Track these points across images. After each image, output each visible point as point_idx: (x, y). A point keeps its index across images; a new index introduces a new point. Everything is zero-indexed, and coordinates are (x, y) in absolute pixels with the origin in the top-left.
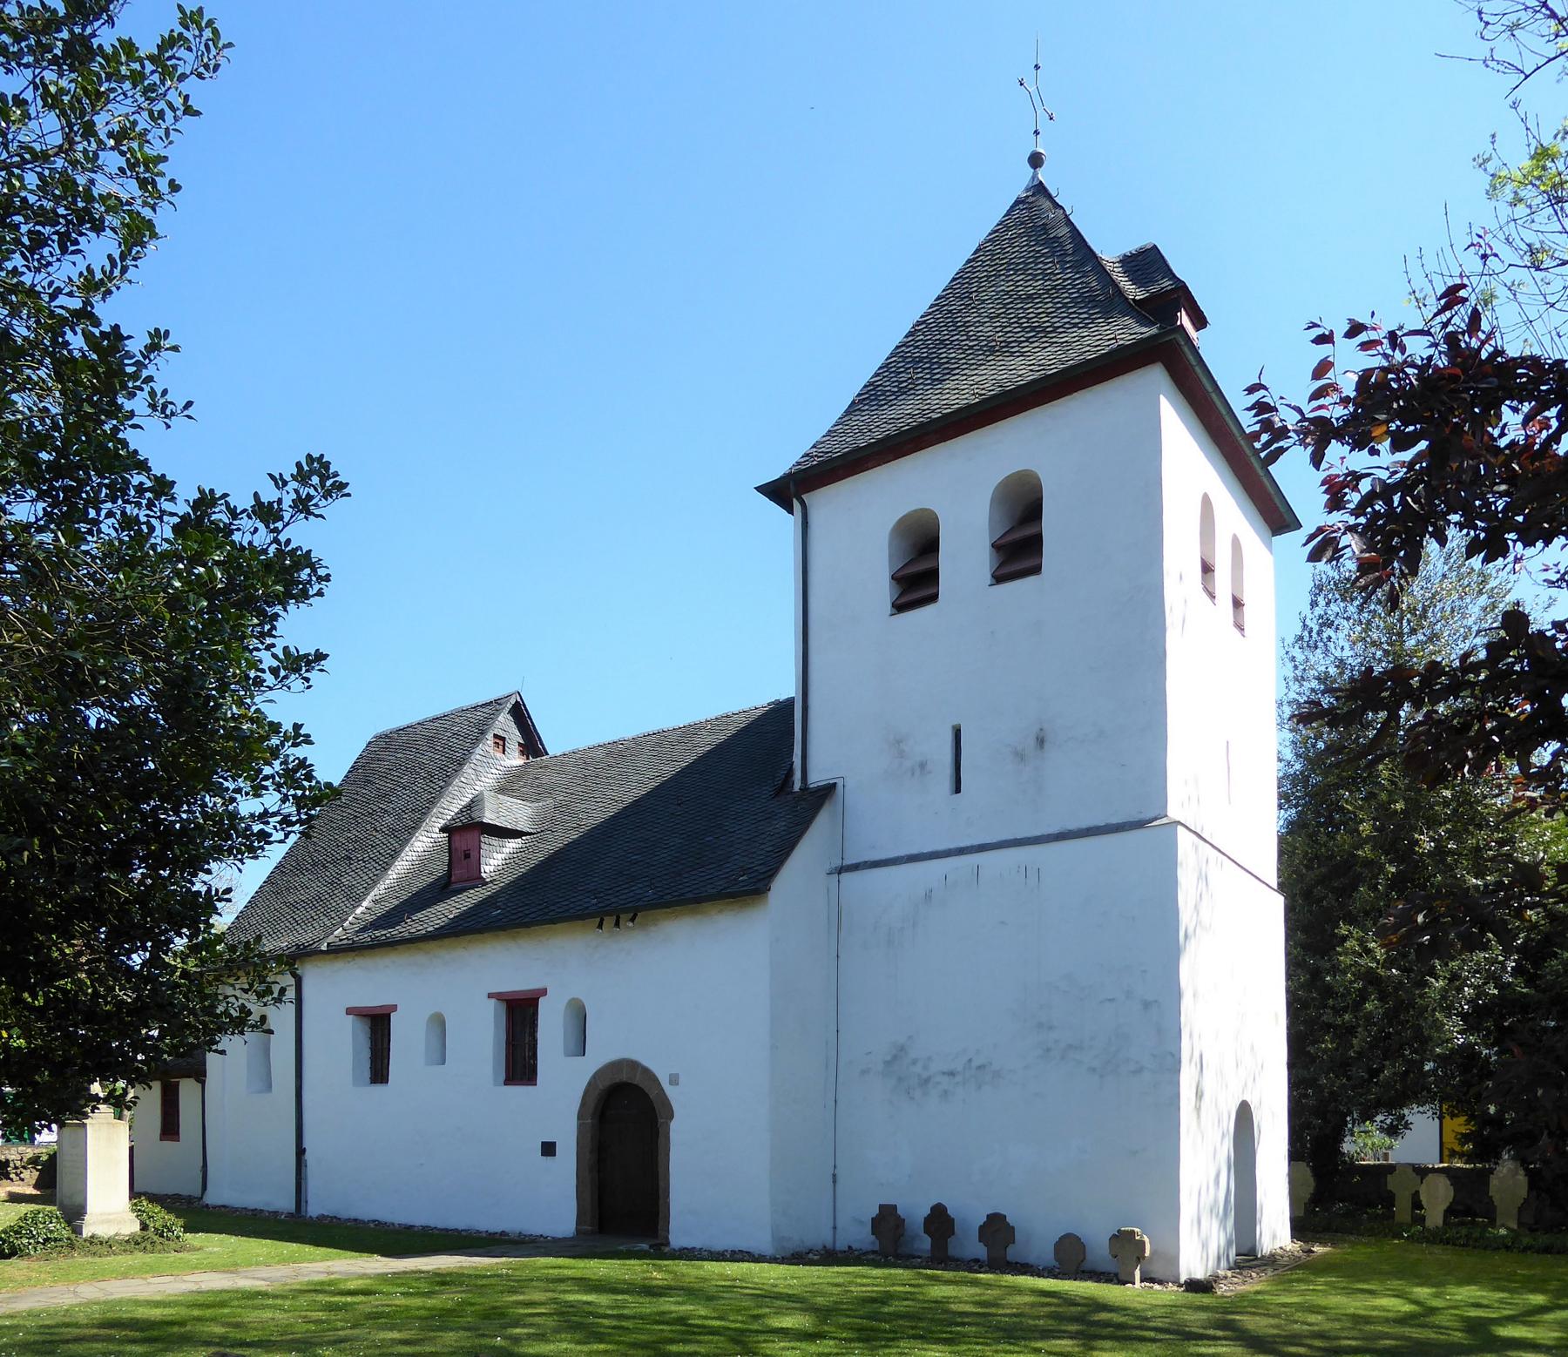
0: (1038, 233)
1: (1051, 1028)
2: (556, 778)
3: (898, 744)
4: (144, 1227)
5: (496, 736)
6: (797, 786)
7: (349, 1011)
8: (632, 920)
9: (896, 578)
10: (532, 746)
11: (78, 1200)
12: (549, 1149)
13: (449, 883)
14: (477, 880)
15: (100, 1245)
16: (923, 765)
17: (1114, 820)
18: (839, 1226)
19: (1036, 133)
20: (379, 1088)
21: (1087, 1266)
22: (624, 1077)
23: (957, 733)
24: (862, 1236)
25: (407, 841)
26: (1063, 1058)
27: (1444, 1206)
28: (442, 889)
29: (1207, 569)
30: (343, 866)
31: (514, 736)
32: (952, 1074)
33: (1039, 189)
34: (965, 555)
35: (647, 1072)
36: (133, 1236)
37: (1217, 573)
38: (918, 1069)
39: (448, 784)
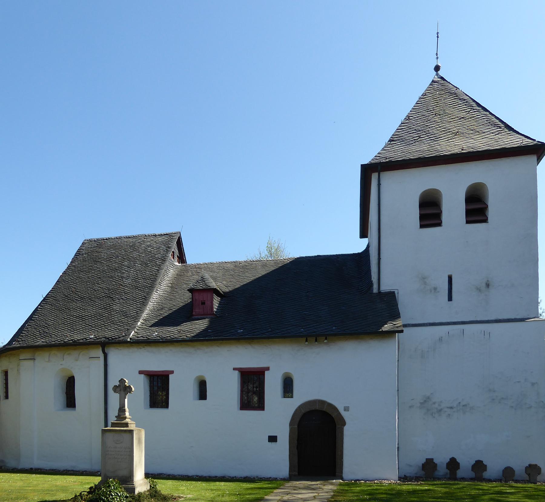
3: (424, 279)
16: (435, 289)
17: (518, 317)
23: (450, 278)
26: (500, 402)
31: (177, 253)
32: (451, 408)
34: (453, 207)
38: (436, 406)
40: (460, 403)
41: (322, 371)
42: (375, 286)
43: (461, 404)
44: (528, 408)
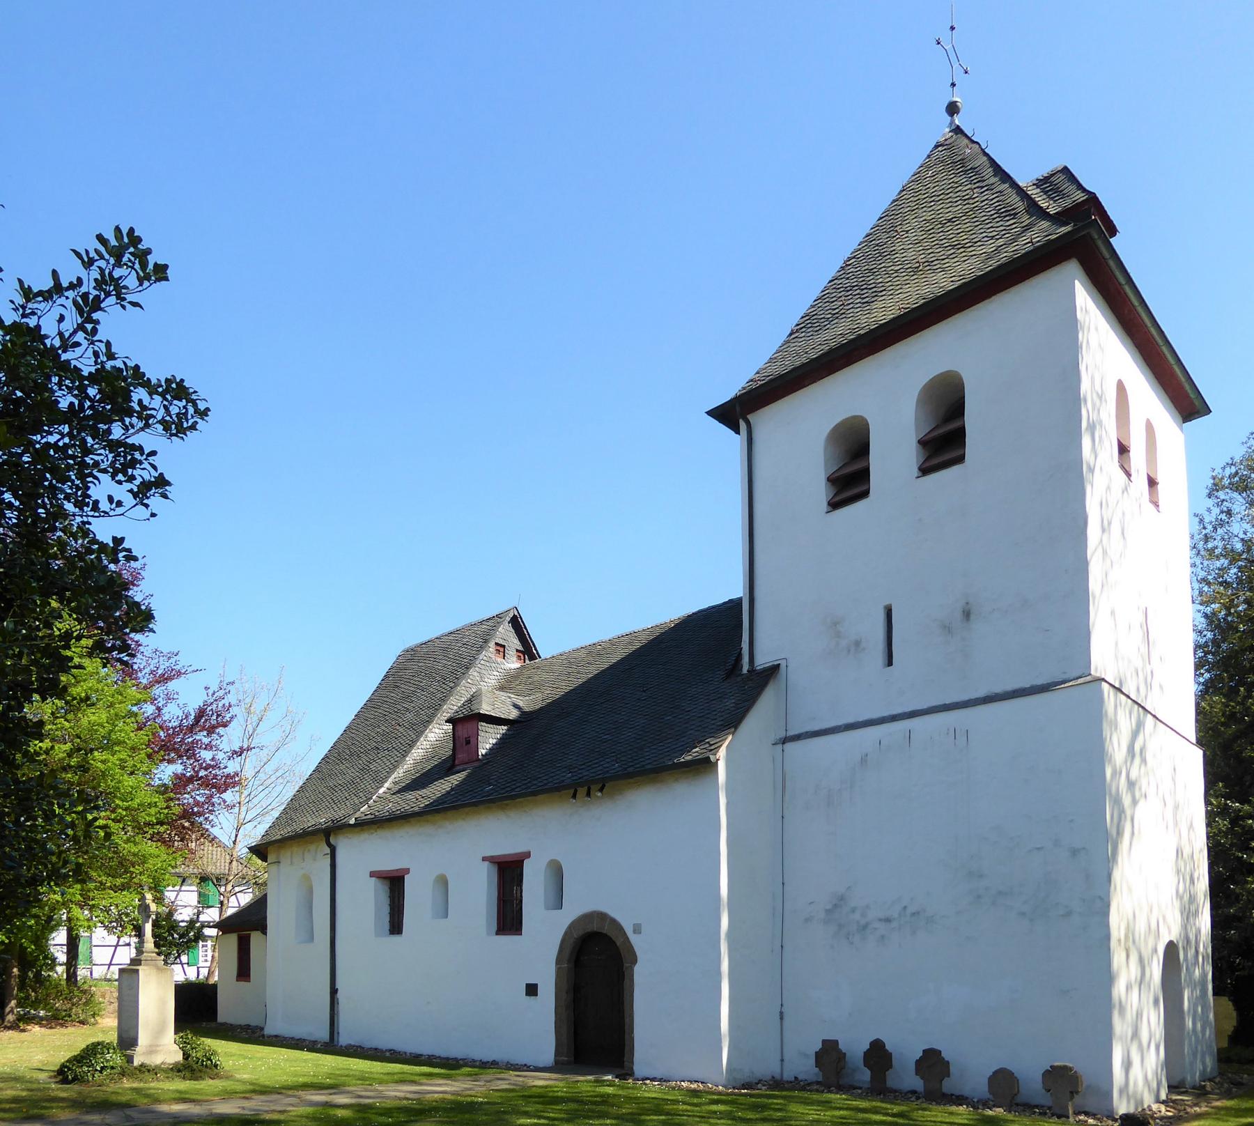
0: (961, 162)
1: (981, 876)
2: (545, 676)
3: (835, 626)
6: (745, 669)
7: (372, 874)
8: (601, 790)
9: (831, 480)
10: (528, 650)
11: (132, 1034)
12: (532, 990)
13: (453, 766)
15: (146, 1070)
17: (1039, 682)
18: (786, 1058)
19: (952, 28)
20: (396, 938)
21: (1019, 1099)
22: (595, 927)
23: (889, 612)
24: (805, 1067)
25: (423, 732)
28: (445, 768)
29: (1123, 450)
30: (372, 755)
31: (514, 643)
32: (888, 920)
33: (958, 130)
34: (894, 453)
35: (614, 922)
36: (176, 1064)
37: (1132, 454)
38: (857, 916)
39: (456, 685)
40: (905, 907)
41: (598, 854)
43: (909, 911)
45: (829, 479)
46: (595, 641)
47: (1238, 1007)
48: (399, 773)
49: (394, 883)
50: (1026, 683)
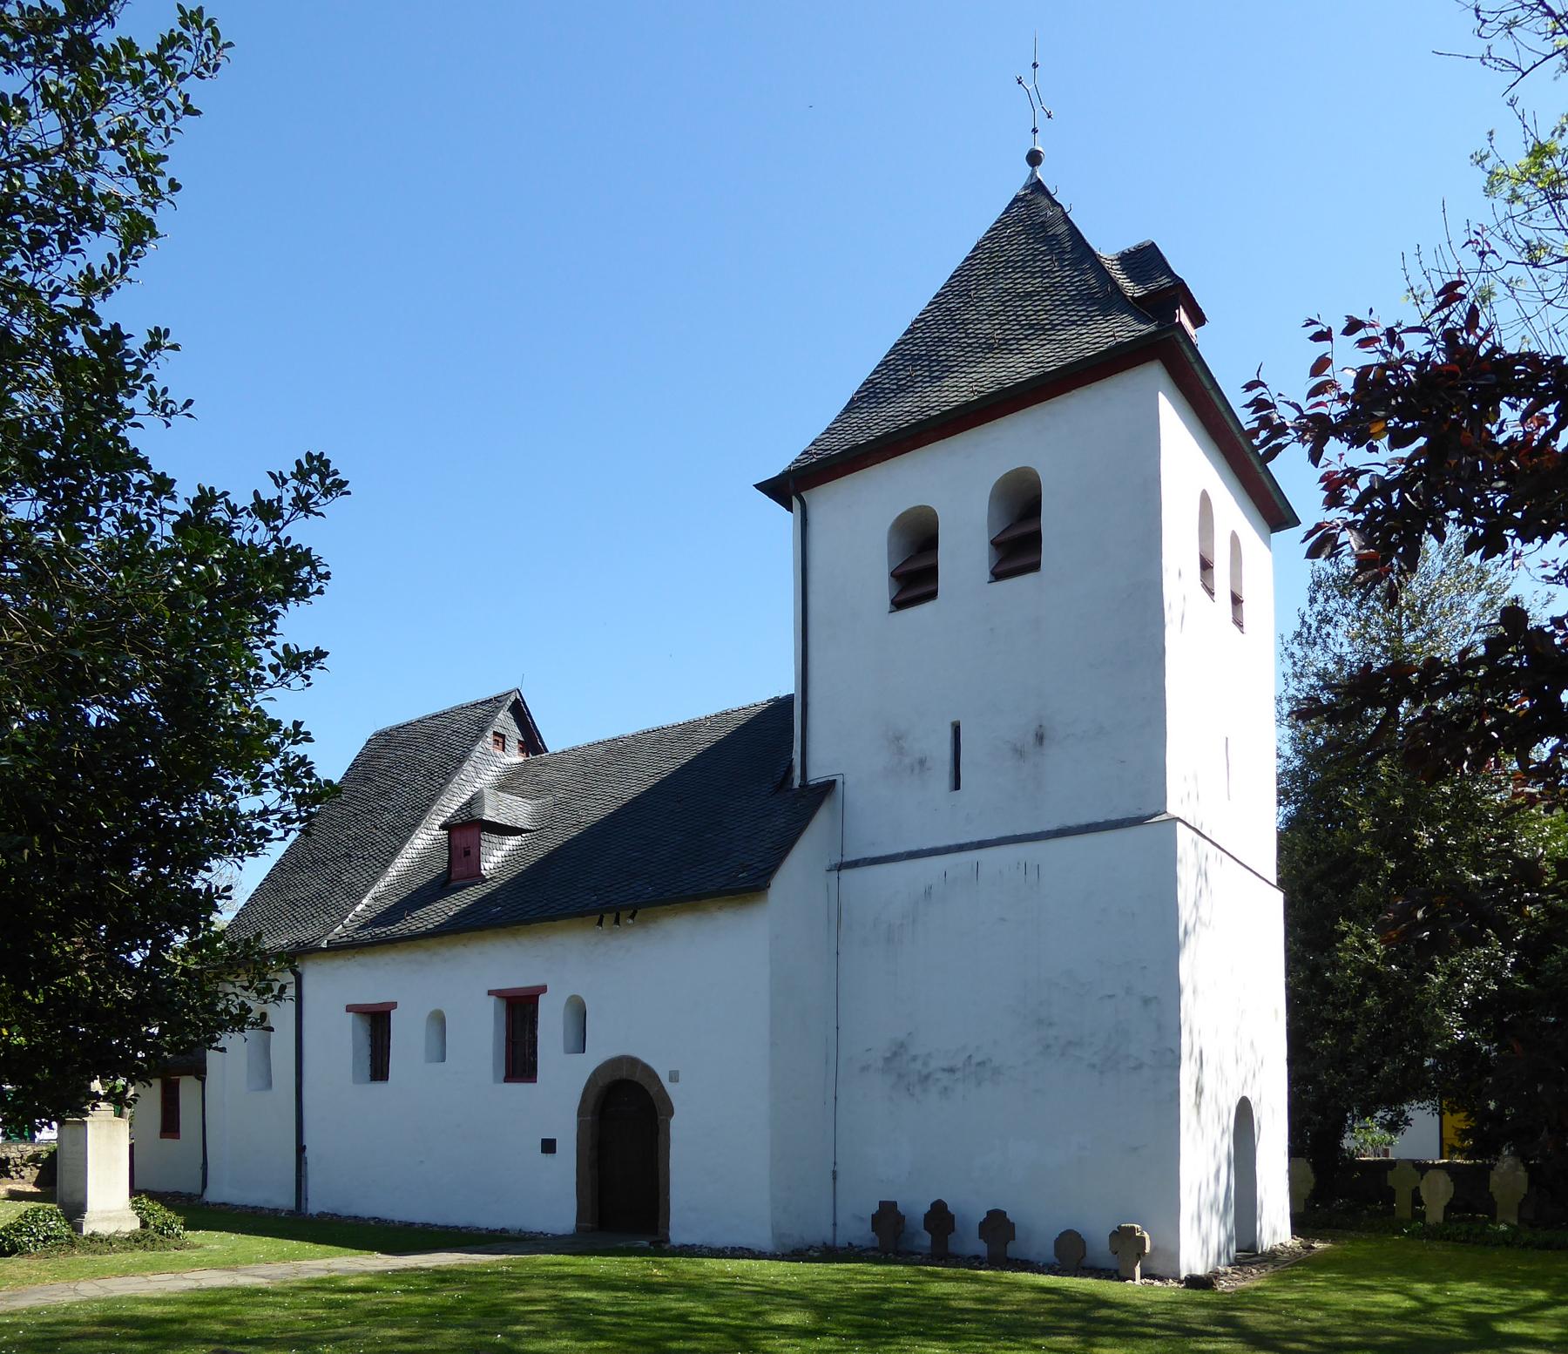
1: (1050, 1024)
3: (897, 740)
4: (144, 1225)
5: (495, 733)
6: (797, 783)
7: (349, 1009)
8: (632, 917)
10: (531, 742)
12: (549, 1146)
13: (449, 880)
14: (477, 877)
15: (100, 1243)
16: (922, 762)
17: (1114, 817)
18: (839, 1222)
22: (624, 1074)
23: (956, 729)
25: (407, 838)
27: (1444, 1203)
28: (441, 887)
29: (1206, 566)
30: (343, 864)
31: (514, 734)
32: (952, 1070)
34: (964, 550)
35: (647, 1069)
36: (133, 1233)
38: (918, 1065)
42: (797, 772)
43: (974, 1061)
44: (1135, 1068)
45: (892, 575)
46: (615, 736)
47: (1316, 1168)
48: (380, 886)
49: (377, 1020)
50: (1100, 818)
